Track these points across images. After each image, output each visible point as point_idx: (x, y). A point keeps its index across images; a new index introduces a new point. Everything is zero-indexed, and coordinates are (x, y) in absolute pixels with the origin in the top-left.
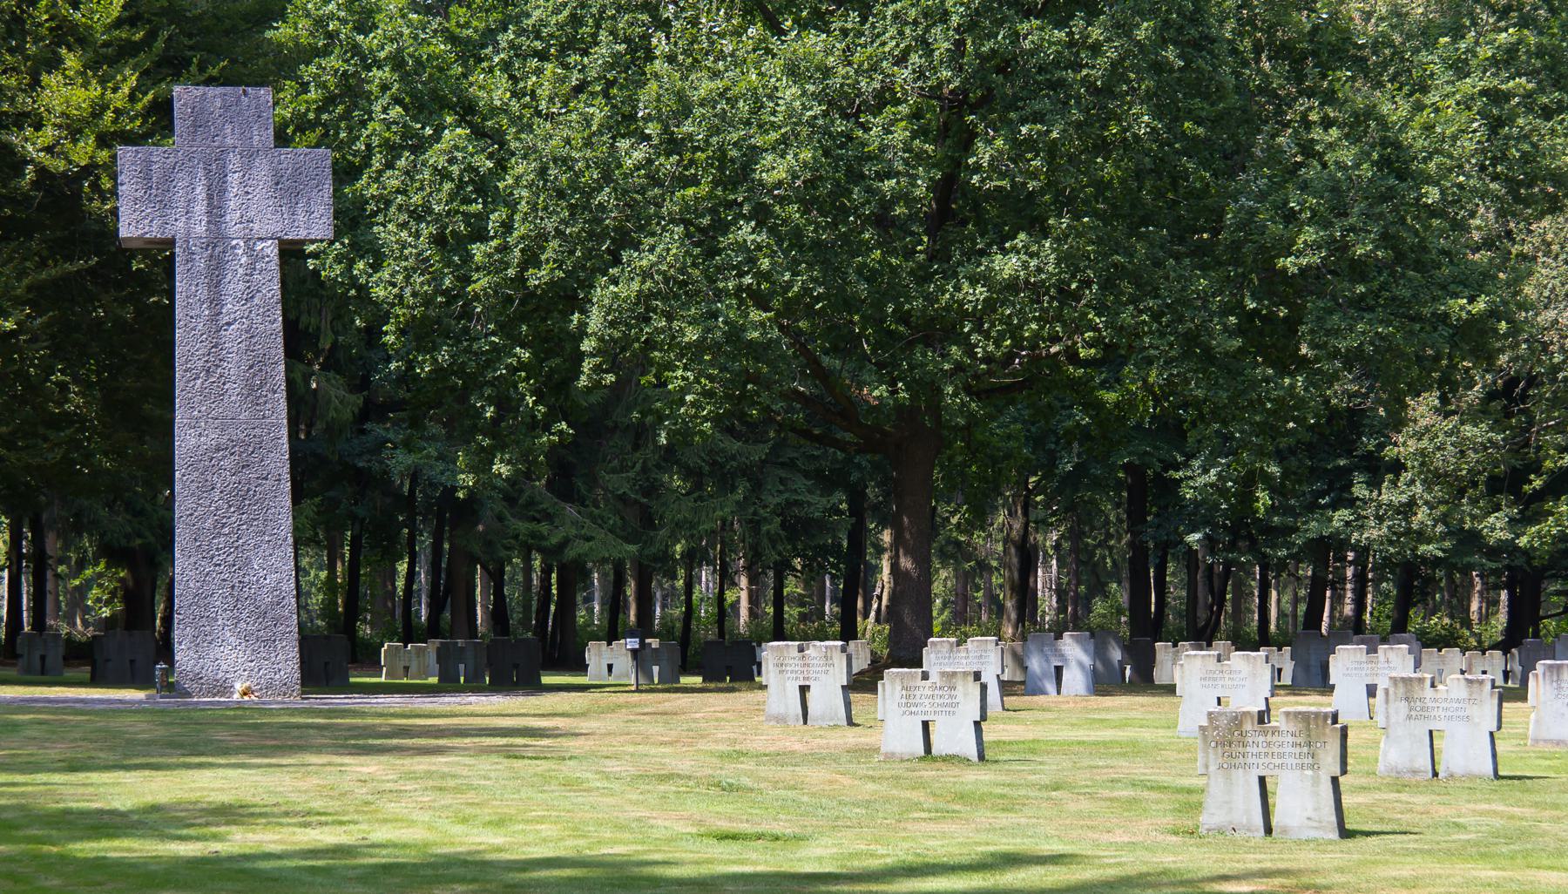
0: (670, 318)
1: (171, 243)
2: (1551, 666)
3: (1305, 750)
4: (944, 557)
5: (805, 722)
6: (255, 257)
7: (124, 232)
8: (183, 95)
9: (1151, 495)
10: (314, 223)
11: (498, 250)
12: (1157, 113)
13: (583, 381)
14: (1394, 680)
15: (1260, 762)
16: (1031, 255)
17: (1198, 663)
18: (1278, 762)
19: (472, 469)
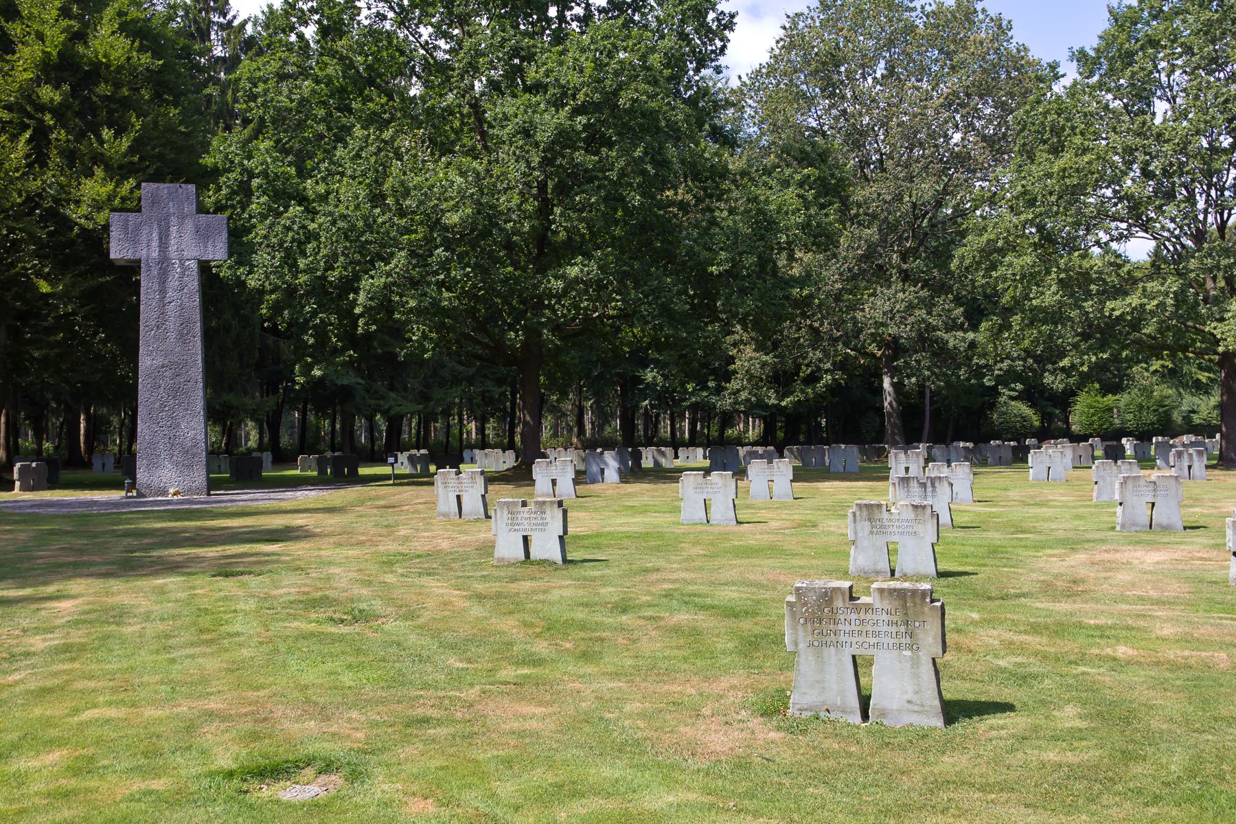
0: (401, 296)
1: (139, 261)
3: (903, 629)
4: (550, 411)
6: (185, 269)
7: (112, 256)
8: (143, 184)
9: (631, 385)
10: (217, 252)
11: (312, 262)
12: (643, 195)
13: (360, 330)
14: (859, 506)
15: (854, 640)
16: (584, 266)
17: (692, 478)
18: (873, 641)
19: (302, 374)
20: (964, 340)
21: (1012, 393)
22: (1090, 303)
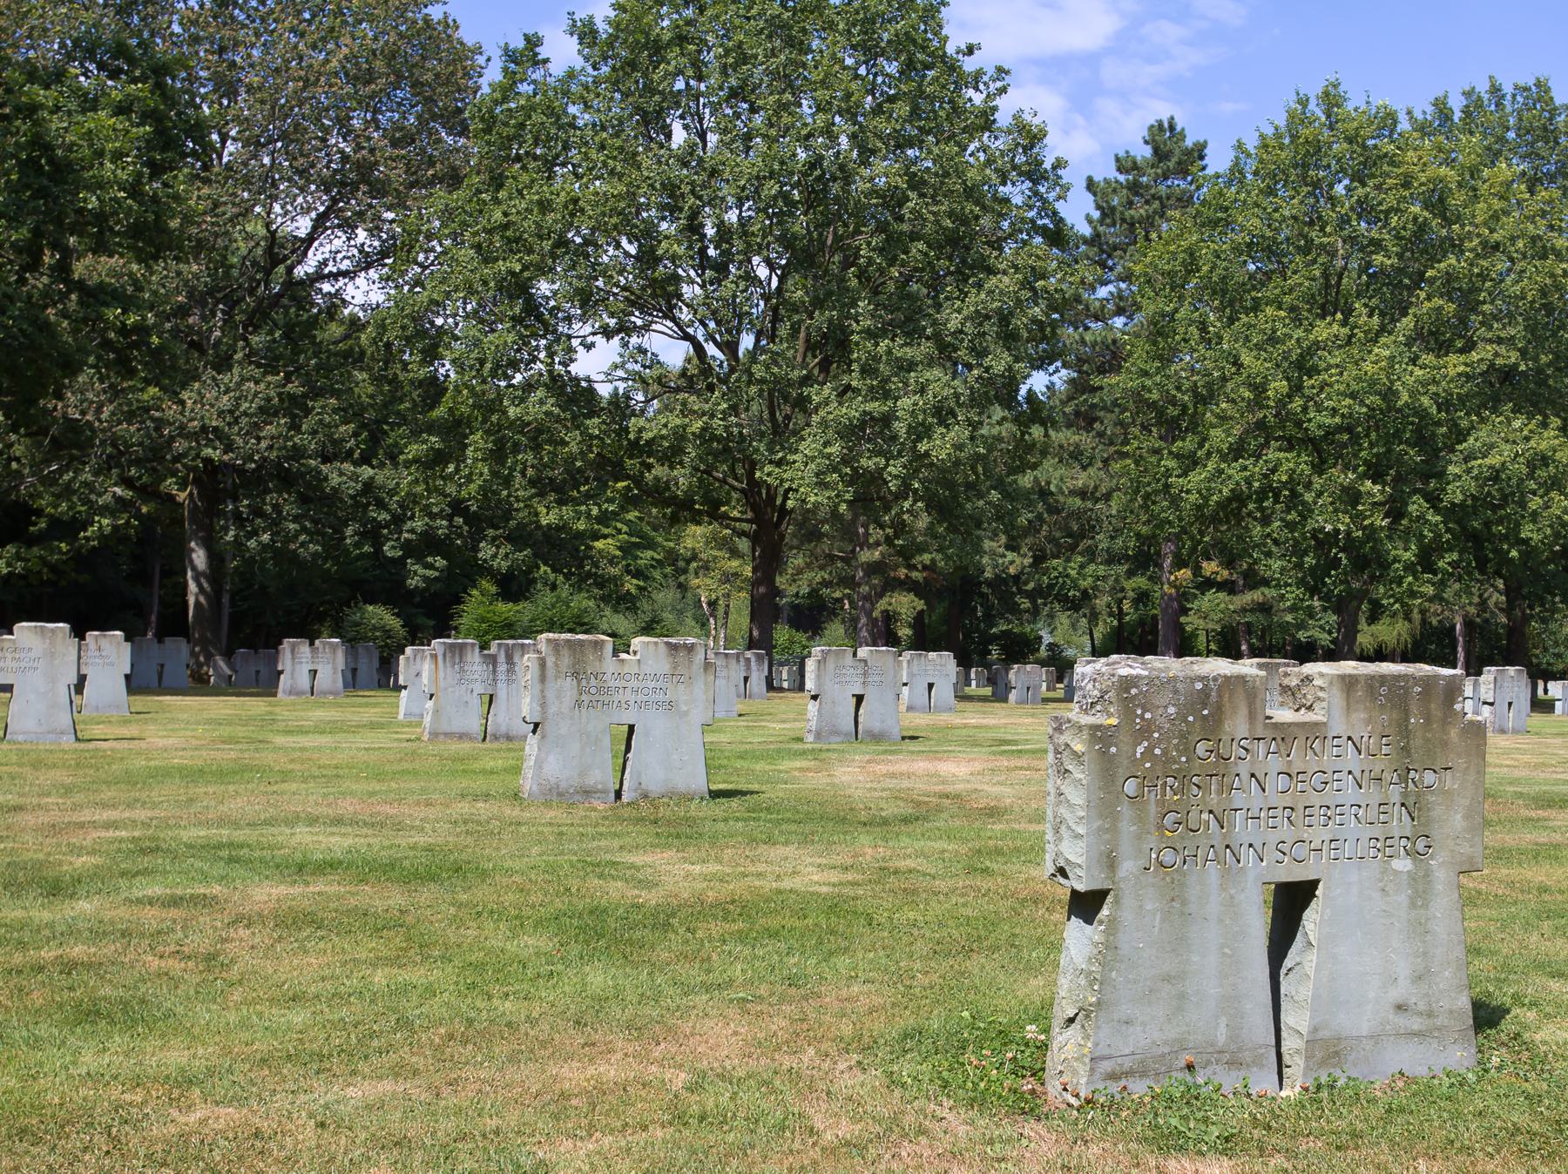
2: (452, 645)
5: (631, 728)
20: (355, 477)
21: (429, 573)
22: (596, 420)
